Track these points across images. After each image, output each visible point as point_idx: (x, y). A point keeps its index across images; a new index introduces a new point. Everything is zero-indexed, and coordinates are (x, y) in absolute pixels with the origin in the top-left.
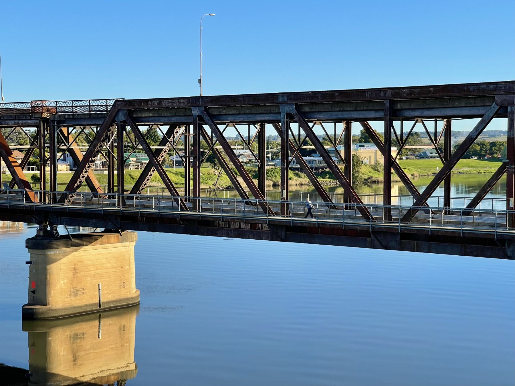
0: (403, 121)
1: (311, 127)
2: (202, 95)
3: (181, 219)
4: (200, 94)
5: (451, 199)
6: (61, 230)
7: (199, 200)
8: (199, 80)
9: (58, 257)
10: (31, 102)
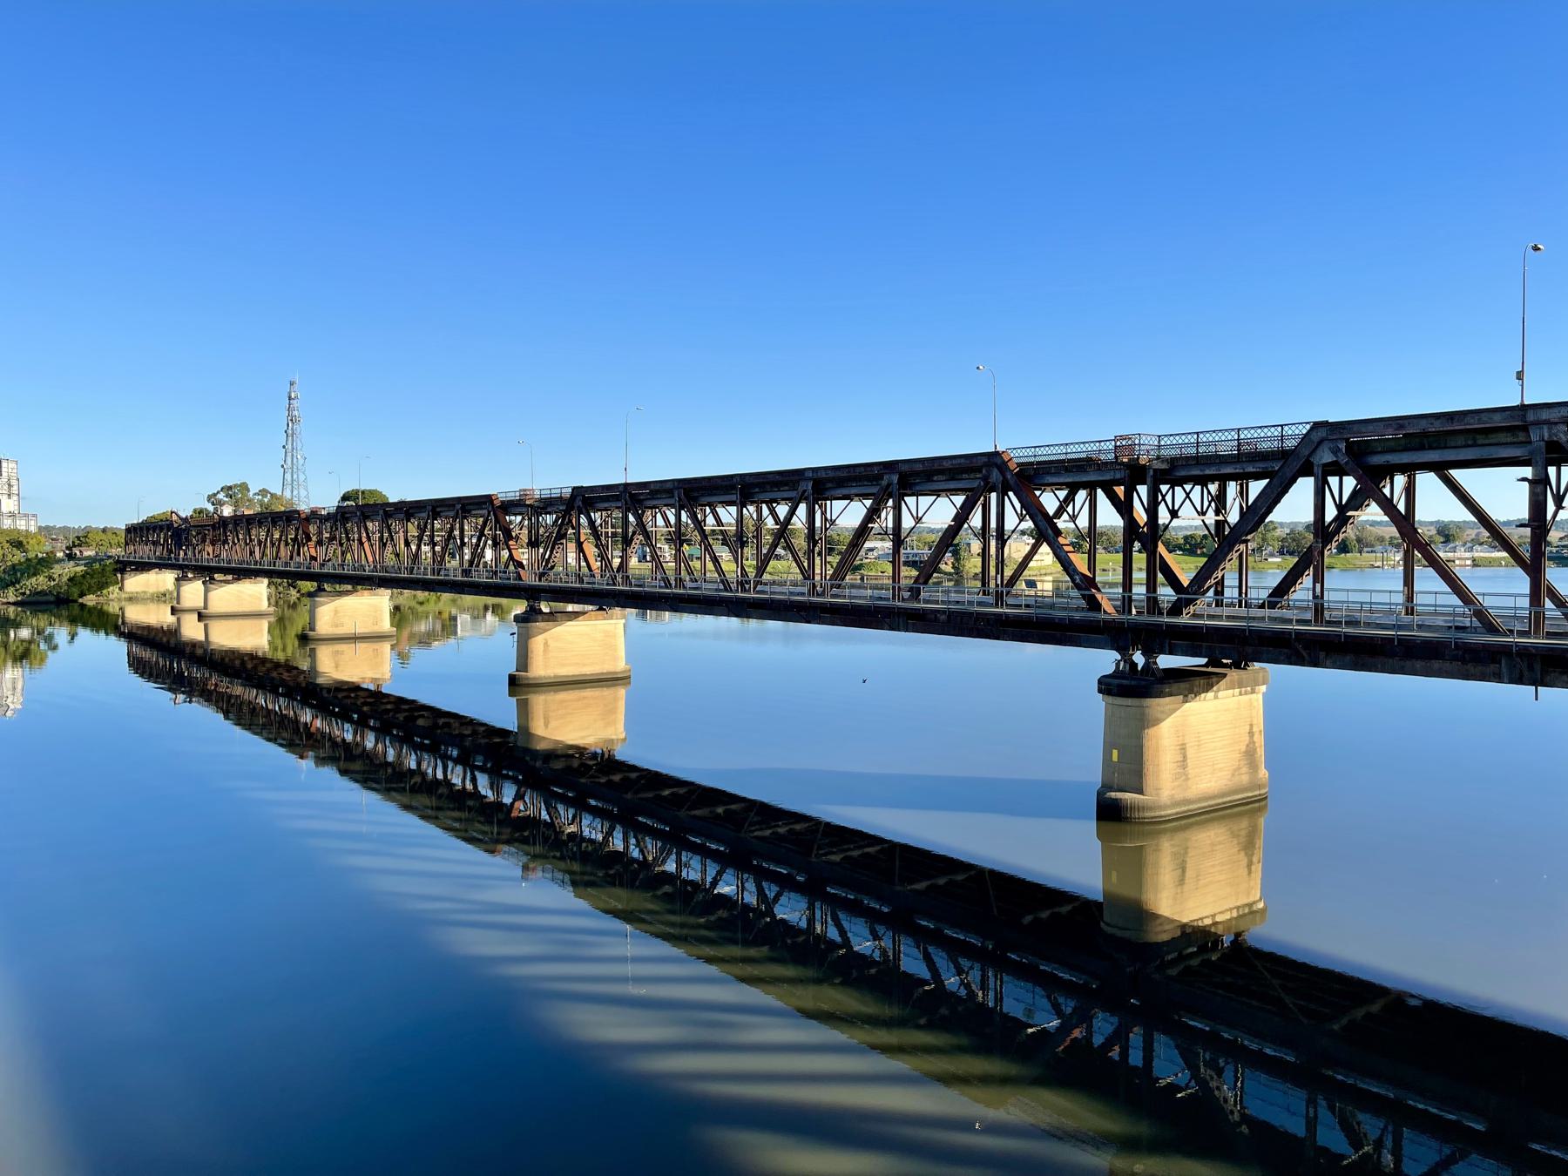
8: (1518, 373)
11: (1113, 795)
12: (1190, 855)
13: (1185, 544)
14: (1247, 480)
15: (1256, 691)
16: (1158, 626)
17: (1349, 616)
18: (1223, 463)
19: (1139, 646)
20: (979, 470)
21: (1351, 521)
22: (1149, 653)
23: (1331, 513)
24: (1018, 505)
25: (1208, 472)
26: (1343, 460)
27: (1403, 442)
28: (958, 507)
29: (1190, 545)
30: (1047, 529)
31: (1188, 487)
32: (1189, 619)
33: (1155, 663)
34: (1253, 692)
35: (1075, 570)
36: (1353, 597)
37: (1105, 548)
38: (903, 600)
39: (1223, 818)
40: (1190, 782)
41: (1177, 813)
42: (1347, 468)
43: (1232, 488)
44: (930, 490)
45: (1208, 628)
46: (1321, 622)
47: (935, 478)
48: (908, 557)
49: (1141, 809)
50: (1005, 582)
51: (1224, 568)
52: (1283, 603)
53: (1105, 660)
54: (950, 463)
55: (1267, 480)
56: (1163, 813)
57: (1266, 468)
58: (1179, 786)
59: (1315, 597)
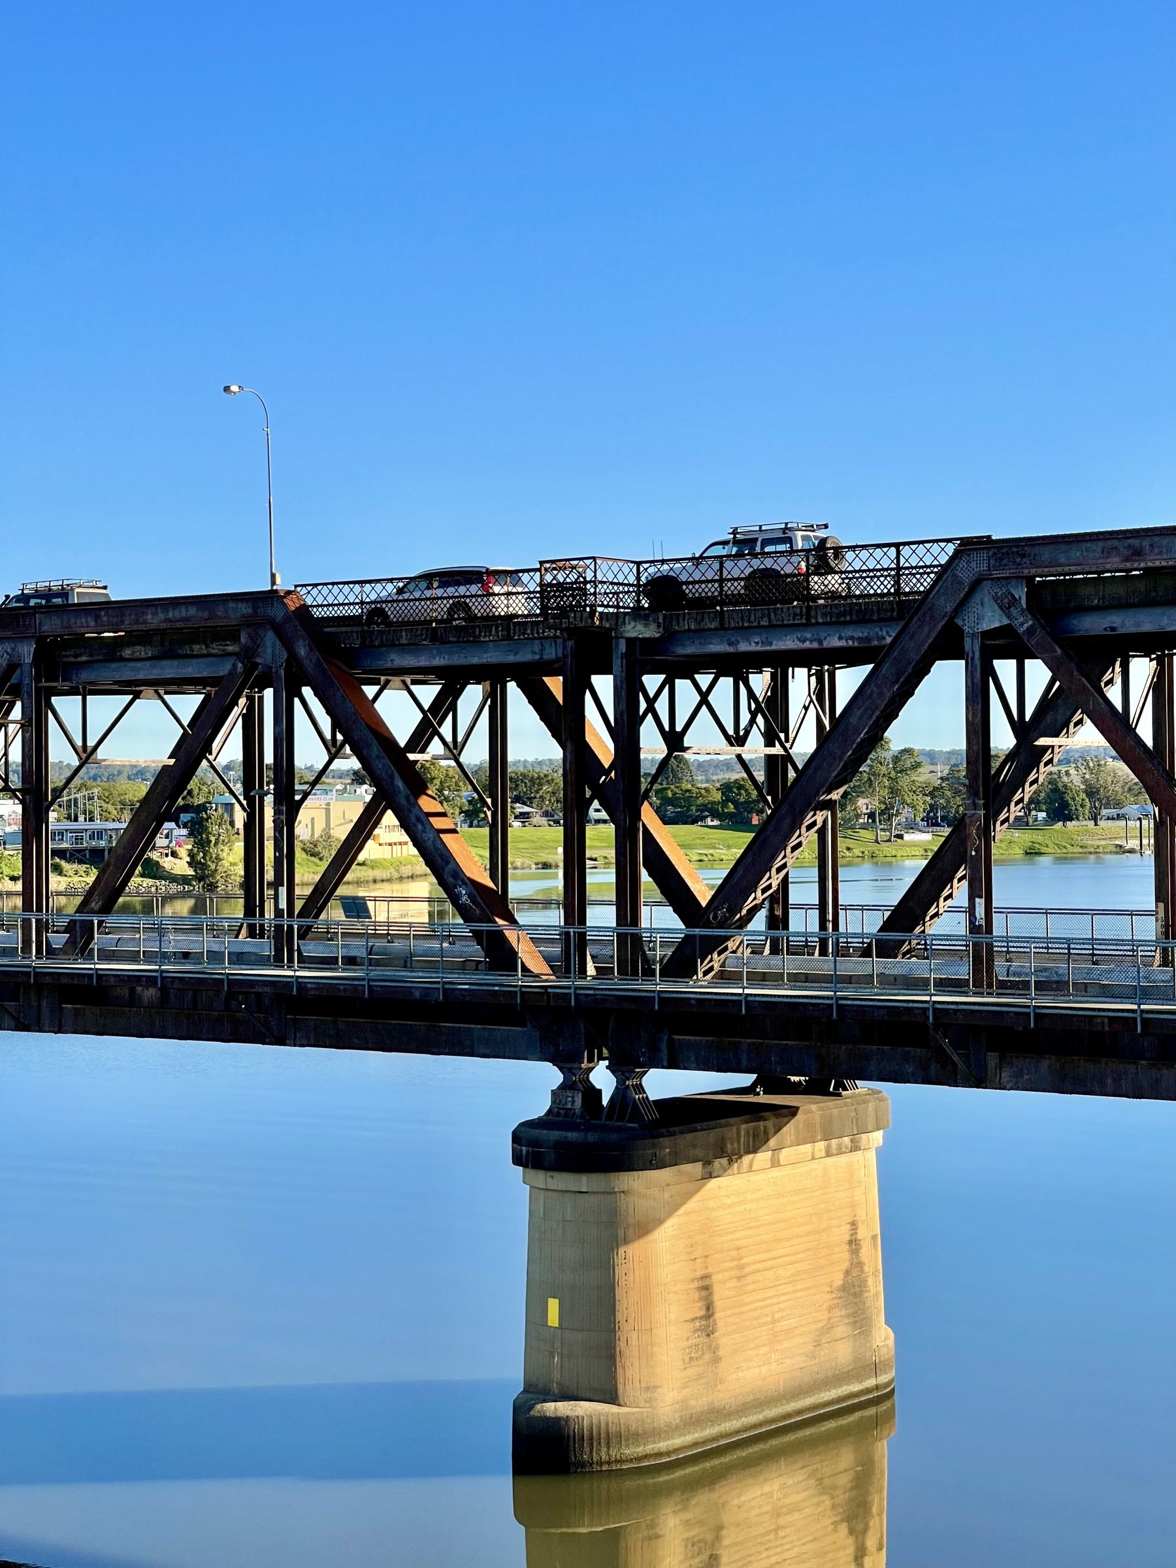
0: (88, 697)
1: (370, 697)
3: (937, 1024)
10: (539, 570)
12: (726, 1542)
13: (724, 803)
14: (831, 664)
15: (863, 1144)
16: (644, 1001)
17: (1045, 969)
18: (776, 626)
19: (605, 1052)
20: (232, 635)
21: (1046, 758)
22: (624, 1067)
23: (1002, 739)
24: (325, 722)
25: (743, 647)
26: (1024, 624)
27: (1142, 587)
28: (186, 724)
29: (735, 803)
30: (392, 777)
31: (704, 680)
32: (711, 984)
33: (640, 1089)
34: (855, 1147)
35: (458, 873)
36: (1061, 928)
37: (546, 814)
38: (51, 952)
39: (813, 1444)
40: (723, 1365)
41: (695, 1444)
42: (1031, 643)
43: (800, 683)
44: (115, 683)
45: (753, 1004)
46: (990, 986)
47: (127, 653)
48: (79, 840)
49: (614, 1440)
50: (298, 905)
51: (784, 866)
52: (914, 942)
54: (162, 616)
55: (870, 667)
56: (663, 1446)
57: (868, 639)
58: (699, 1377)
59: (974, 928)
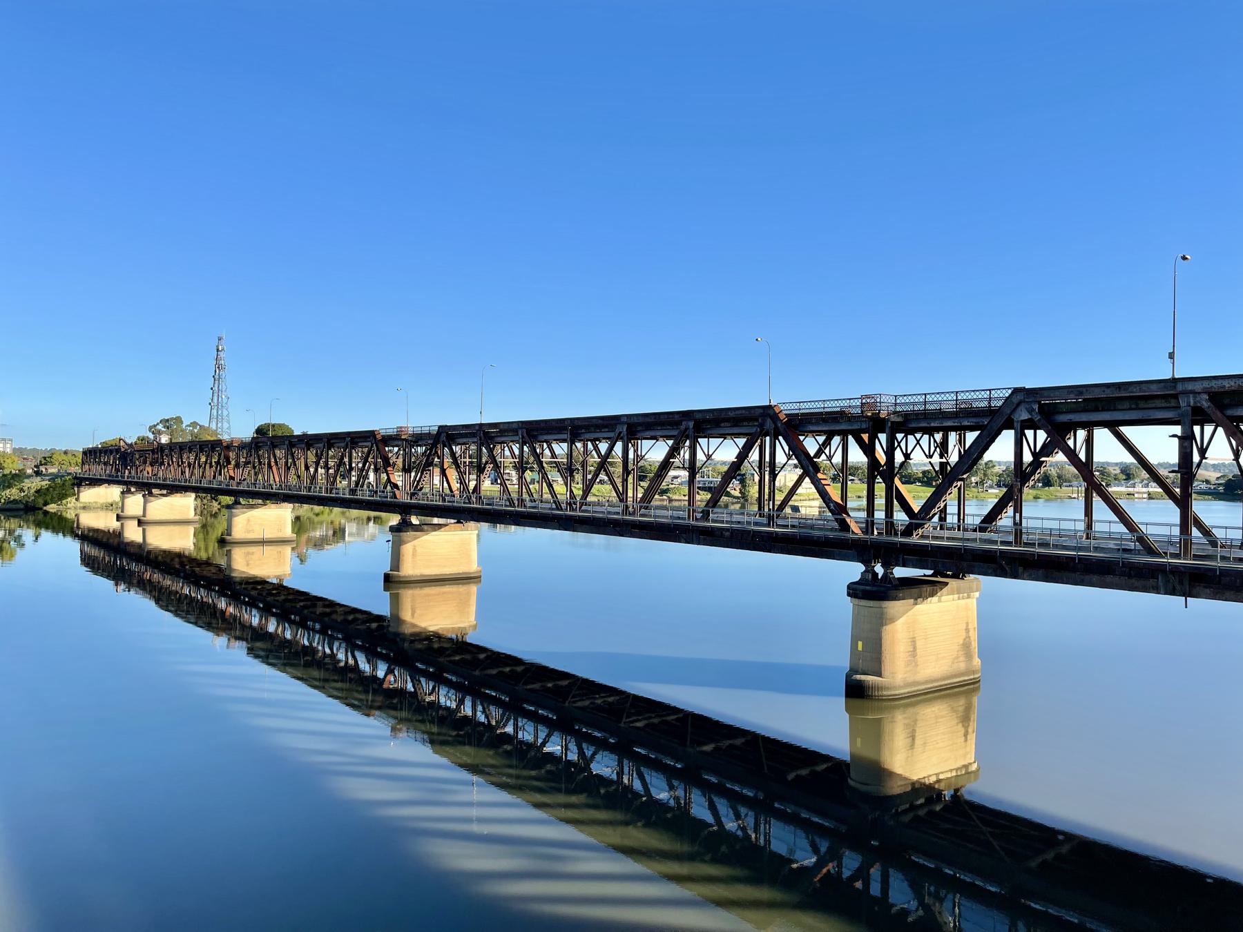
2: (1176, 377)
4: (1172, 374)
5: (1093, 523)
6: (415, 520)
7: (1021, 530)
8: (1170, 353)
9: (409, 539)
11: (858, 677)
53: (854, 570)
